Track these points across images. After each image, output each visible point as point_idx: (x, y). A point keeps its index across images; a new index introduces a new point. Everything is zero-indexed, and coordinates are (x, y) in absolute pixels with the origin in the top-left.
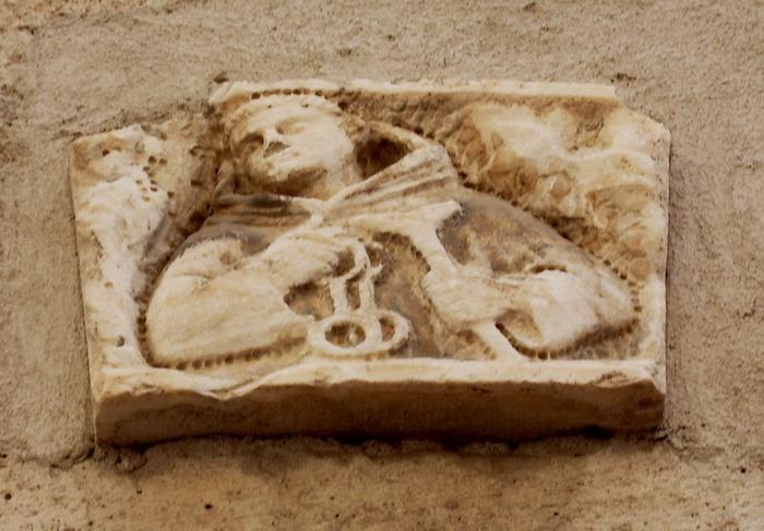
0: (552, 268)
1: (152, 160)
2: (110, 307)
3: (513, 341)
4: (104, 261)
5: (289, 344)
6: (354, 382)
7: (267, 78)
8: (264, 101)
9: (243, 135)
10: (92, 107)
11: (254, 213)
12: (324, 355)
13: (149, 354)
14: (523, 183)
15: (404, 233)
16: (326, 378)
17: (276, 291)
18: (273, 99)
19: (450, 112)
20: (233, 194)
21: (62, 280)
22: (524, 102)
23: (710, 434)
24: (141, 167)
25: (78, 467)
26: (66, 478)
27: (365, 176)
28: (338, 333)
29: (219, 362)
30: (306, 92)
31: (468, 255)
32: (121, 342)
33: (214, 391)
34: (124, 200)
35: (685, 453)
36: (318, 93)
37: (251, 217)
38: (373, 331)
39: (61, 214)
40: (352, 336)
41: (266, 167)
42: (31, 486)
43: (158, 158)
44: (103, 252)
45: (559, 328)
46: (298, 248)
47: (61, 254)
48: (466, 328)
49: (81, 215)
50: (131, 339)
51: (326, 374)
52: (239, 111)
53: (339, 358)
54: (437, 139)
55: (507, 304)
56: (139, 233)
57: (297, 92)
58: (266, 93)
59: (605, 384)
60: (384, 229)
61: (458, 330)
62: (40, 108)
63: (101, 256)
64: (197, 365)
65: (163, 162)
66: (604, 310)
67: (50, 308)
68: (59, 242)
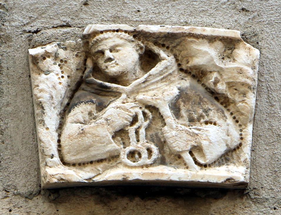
0: (211, 123)
1: (61, 61)
2: (48, 136)
3: (195, 160)
4: (45, 116)
5: (113, 158)
6: (137, 180)
7: (110, 140)
8: (105, 35)
9: (96, 50)
10: (35, 17)
11: (100, 90)
12: (126, 165)
13: (62, 157)
14: (202, 74)
15: (158, 107)
16: (127, 177)
17: (109, 134)
18: (109, 34)
19: (176, 39)
20: (92, 83)
21: (27, 109)
22: (204, 38)
23: (264, 192)
24: (57, 65)
25: (35, 198)
26: (31, 203)
27: (146, 72)
28: (132, 154)
29: (88, 163)
30: (122, 31)
31: (180, 115)
32: (52, 157)
33: (86, 180)
34: (52, 84)
35: (255, 200)
36: (126, 32)
37: (99, 92)
38: (145, 154)
39: (25, 75)
40: (137, 156)
41: (105, 68)
42: (19, 206)
43: (64, 60)
44: (45, 111)
45: (213, 152)
46: (118, 111)
47: (25, 95)
48: (178, 153)
49: (36, 91)
50: (56, 153)
51: (127, 176)
52: (95, 39)
53: (132, 167)
54: (170, 49)
55: (193, 143)
56: (57, 101)
57: (117, 31)
58: (106, 31)
59: (228, 183)
60: (149, 104)
61: (175, 154)
62: (15, 16)
63: (44, 113)
64: (80, 164)
65: (66, 62)
66: (229, 142)
67: (23, 122)
68: (25, 90)
